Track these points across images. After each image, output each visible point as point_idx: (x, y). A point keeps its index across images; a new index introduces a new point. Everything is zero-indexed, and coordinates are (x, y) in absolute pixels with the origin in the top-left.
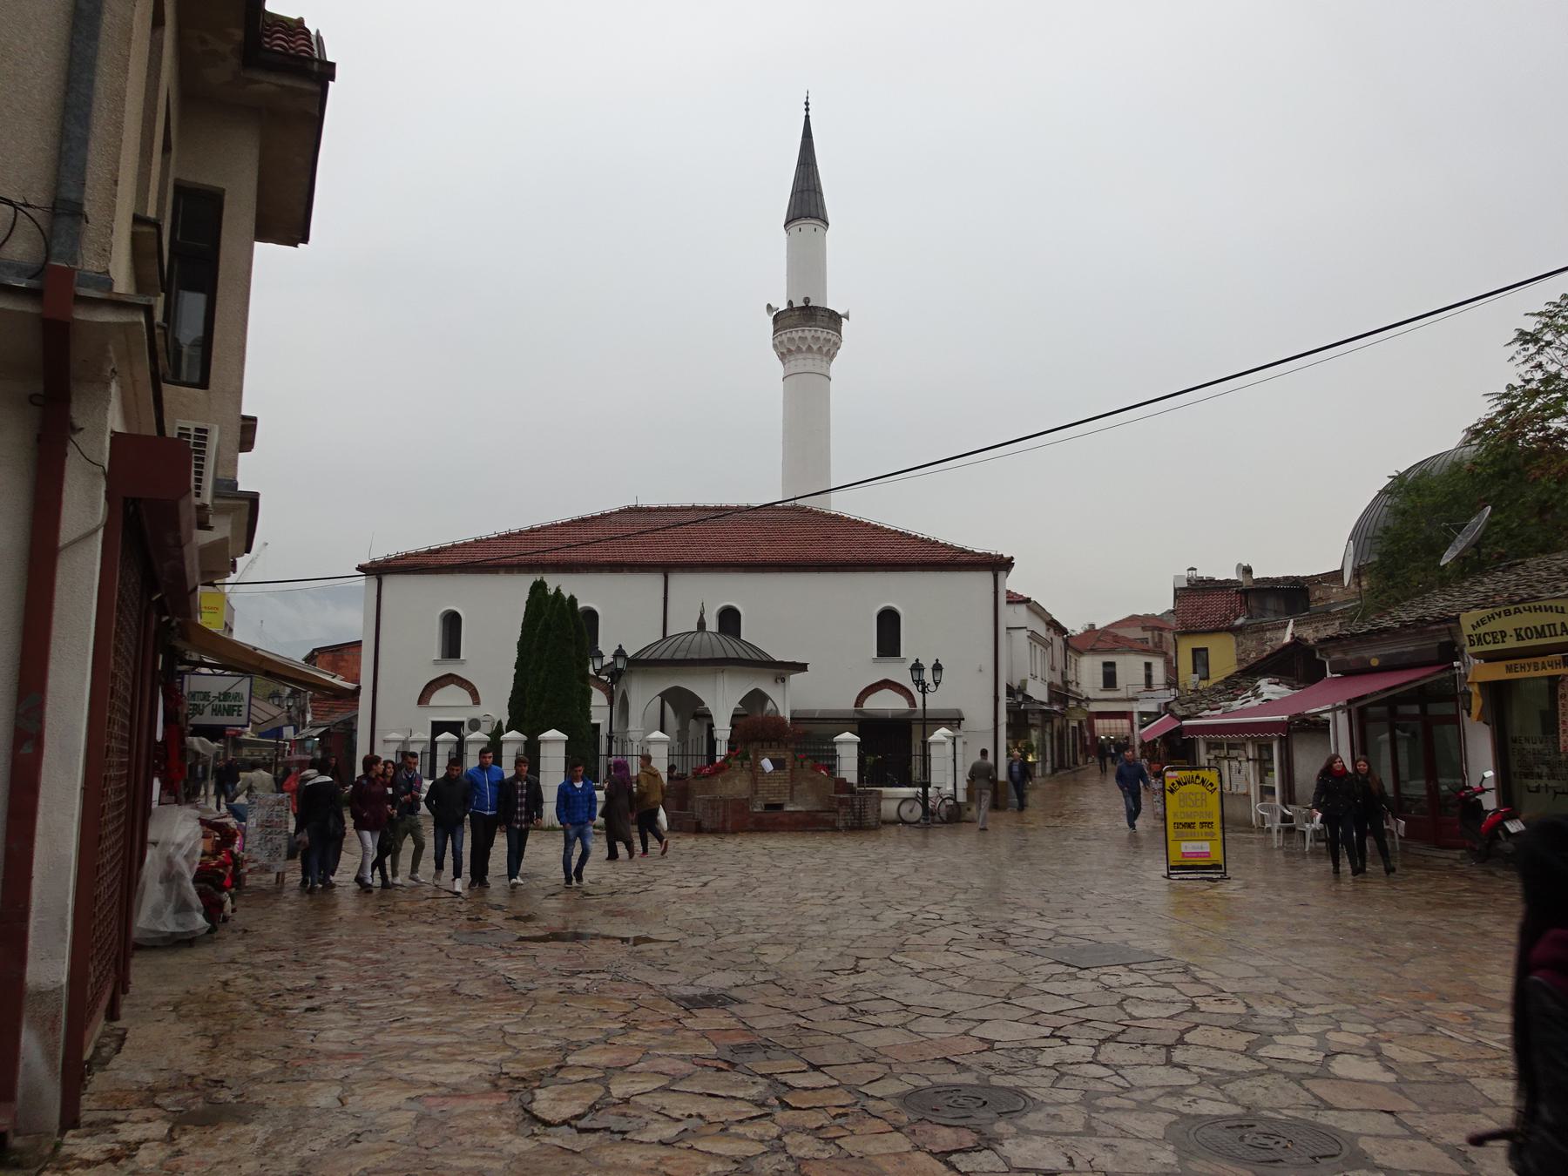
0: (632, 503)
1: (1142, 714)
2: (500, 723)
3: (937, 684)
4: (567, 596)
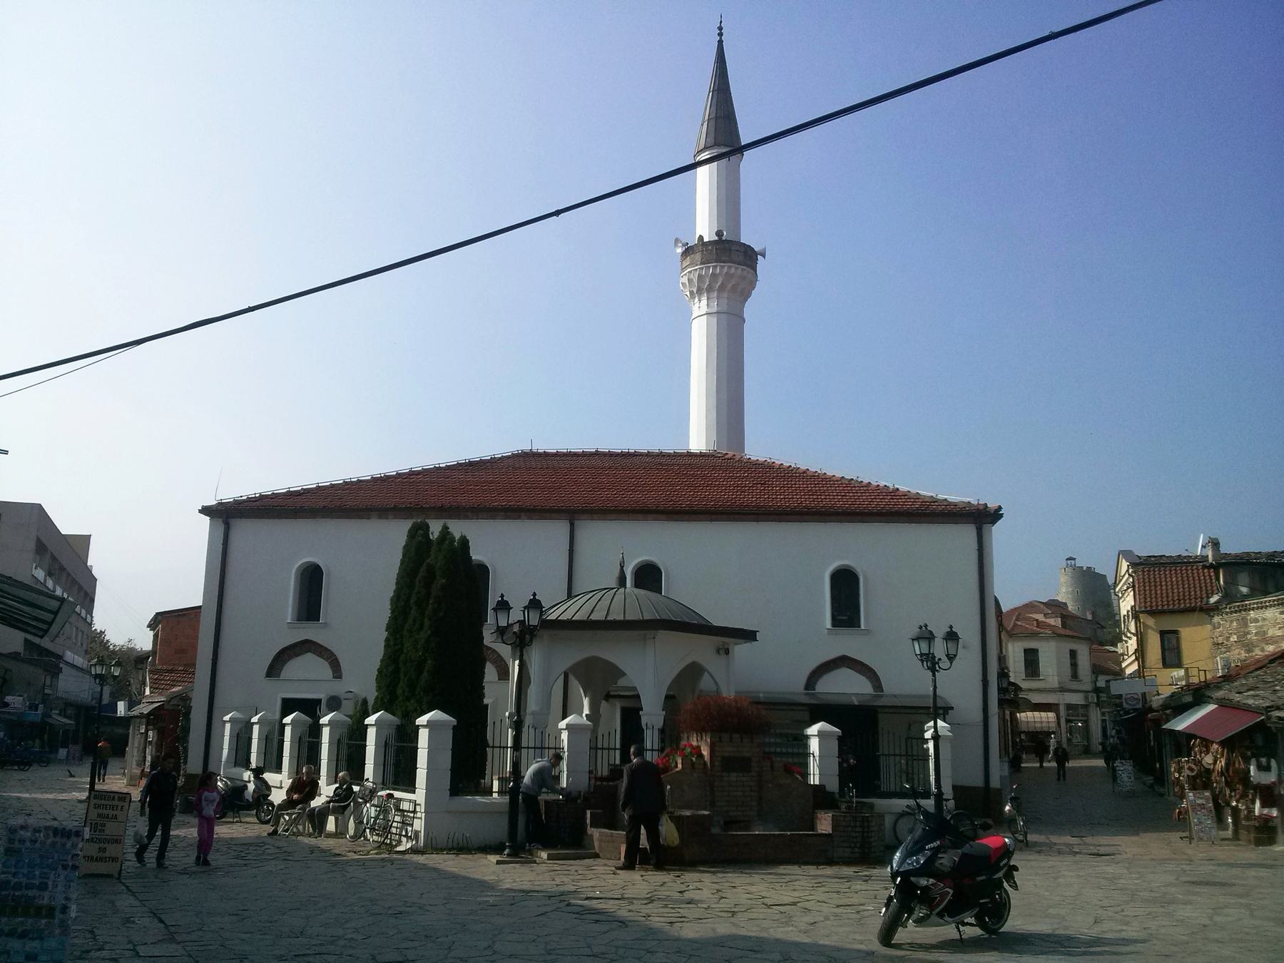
0: (527, 448)
1: (1069, 707)
2: (365, 702)
3: (951, 658)
4: (457, 537)
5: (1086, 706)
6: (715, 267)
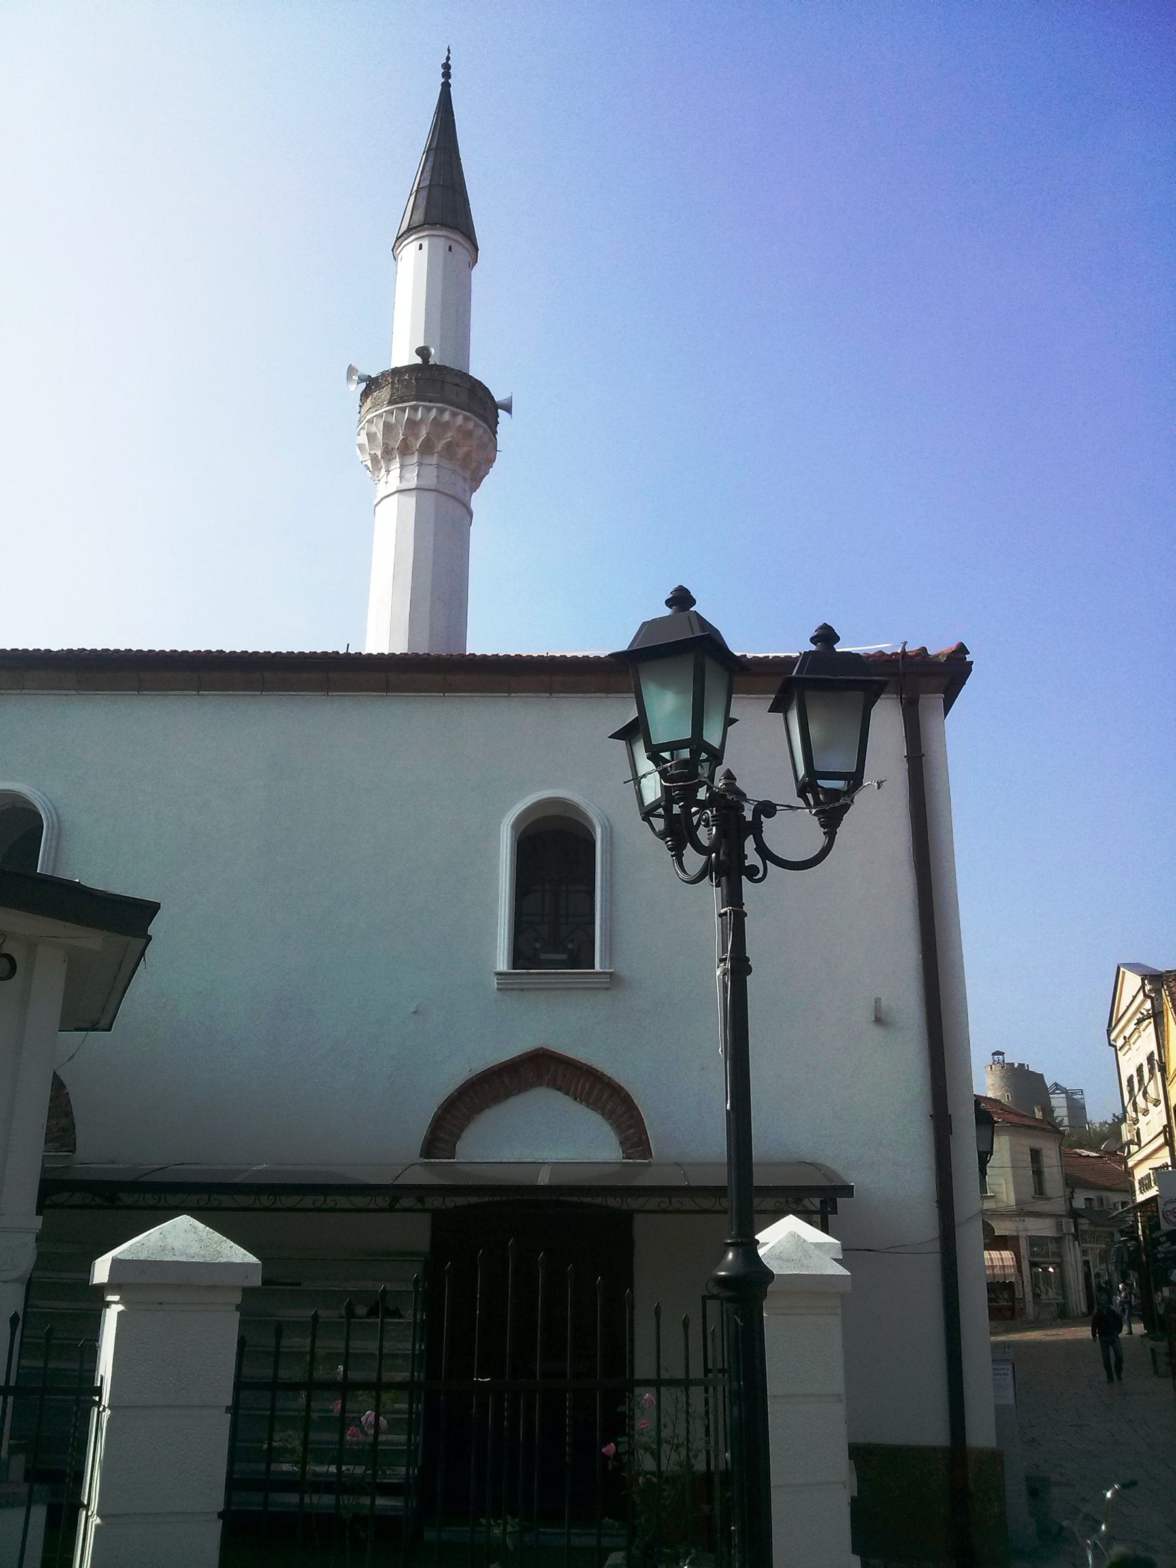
1: (1034, 1241)
5: (1058, 1240)
6: (415, 409)
